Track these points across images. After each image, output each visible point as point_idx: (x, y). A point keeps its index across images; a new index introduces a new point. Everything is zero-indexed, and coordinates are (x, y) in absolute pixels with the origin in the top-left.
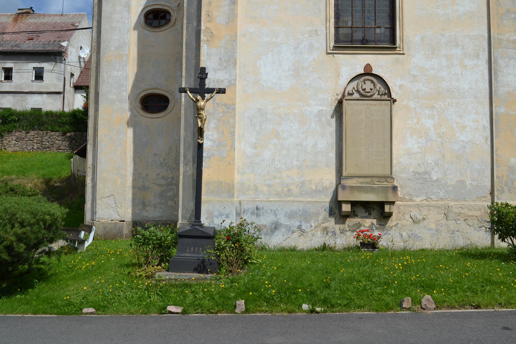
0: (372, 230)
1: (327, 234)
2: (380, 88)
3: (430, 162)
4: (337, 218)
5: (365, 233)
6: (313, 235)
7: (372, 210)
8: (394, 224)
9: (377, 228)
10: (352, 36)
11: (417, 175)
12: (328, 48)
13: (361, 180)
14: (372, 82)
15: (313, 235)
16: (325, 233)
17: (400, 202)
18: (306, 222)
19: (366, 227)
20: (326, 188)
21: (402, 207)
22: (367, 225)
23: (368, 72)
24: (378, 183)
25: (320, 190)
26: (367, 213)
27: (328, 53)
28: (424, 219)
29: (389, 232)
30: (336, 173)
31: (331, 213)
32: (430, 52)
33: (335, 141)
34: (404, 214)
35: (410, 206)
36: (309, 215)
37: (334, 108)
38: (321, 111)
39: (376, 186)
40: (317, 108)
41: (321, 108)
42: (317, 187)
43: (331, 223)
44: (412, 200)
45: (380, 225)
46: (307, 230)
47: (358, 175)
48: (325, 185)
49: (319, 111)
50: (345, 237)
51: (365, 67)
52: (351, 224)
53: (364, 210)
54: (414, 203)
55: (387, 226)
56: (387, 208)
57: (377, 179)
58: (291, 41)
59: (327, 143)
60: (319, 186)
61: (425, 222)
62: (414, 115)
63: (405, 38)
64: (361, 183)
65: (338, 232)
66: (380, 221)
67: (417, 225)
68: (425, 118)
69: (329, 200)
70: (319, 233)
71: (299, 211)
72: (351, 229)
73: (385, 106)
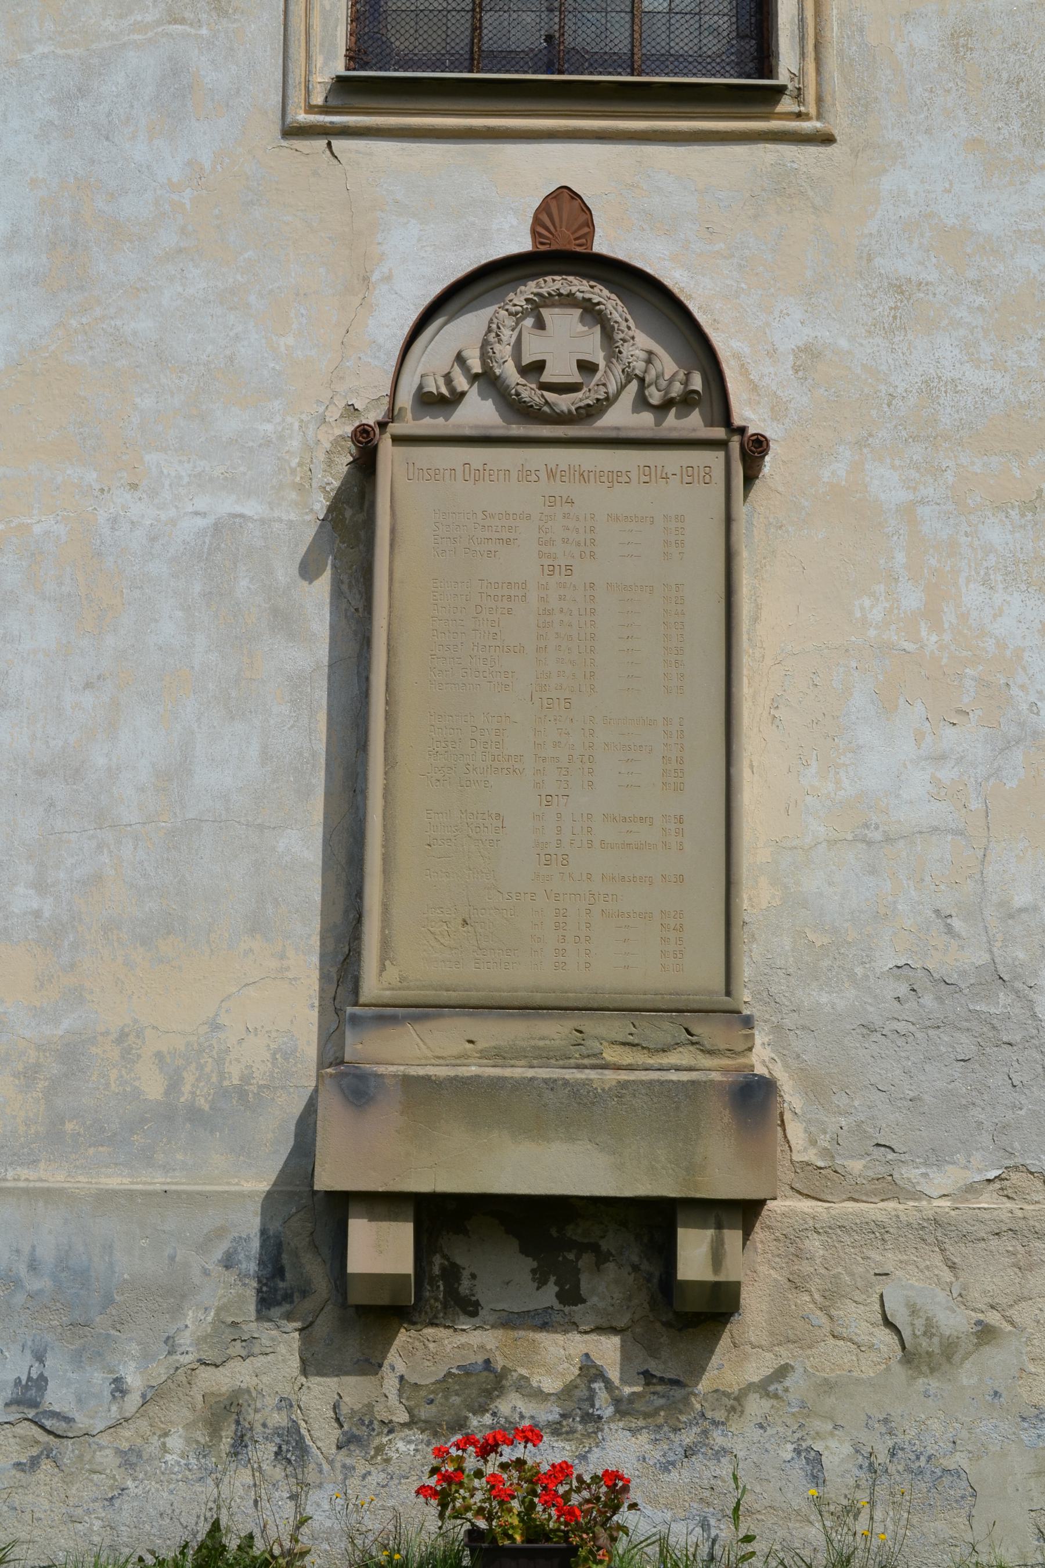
0: (588, 1418)
1: (240, 1443)
2: (650, 355)
3: (1022, 898)
4: (323, 1326)
5: (508, 1453)
6: (130, 1459)
7: (587, 1260)
8: (756, 1370)
9: (623, 1408)
10: (476, 28)
11: (928, 1000)
12: (297, 98)
13: (495, 1032)
14: (591, 312)
15: (130, 1459)
16: (226, 1443)
17: (806, 1205)
18: (78, 1359)
19: (539, 1395)
20: (241, 1093)
21: (814, 1244)
22: (551, 1385)
23: (562, 251)
24: (627, 1057)
25: (202, 1103)
26: (551, 1289)
27: (293, 132)
28: (985, 1333)
29: (718, 1438)
30: (324, 977)
31: (276, 1288)
32: (1016, 126)
33: (321, 746)
34: (831, 1297)
35: (878, 1232)
36: (108, 1300)
37: (320, 505)
38: (226, 529)
39: (610, 1075)
40: (201, 503)
41: (228, 505)
42: (174, 1085)
43: (273, 1365)
44: (890, 1188)
45: (648, 1377)
46: (82, 1422)
47: (475, 997)
48: (235, 1072)
49: (217, 528)
50: (377, 1477)
51: (545, 207)
52: (428, 1374)
53: (522, 1267)
54: (905, 1209)
55: (704, 1386)
56: (694, 1255)
57: (617, 1027)
58: (40, 49)
59: (265, 756)
60: (189, 1077)
61: (996, 1359)
62: (900, 557)
63: (834, 31)
64: (498, 1055)
65: (322, 1436)
66: (653, 1352)
67: (934, 1384)
68: (985, 582)
69: (264, 1187)
70: (175, 1442)
71: (33, 1266)
72: (425, 1412)
73: (688, 484)
